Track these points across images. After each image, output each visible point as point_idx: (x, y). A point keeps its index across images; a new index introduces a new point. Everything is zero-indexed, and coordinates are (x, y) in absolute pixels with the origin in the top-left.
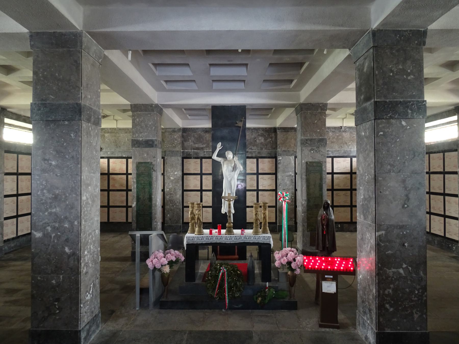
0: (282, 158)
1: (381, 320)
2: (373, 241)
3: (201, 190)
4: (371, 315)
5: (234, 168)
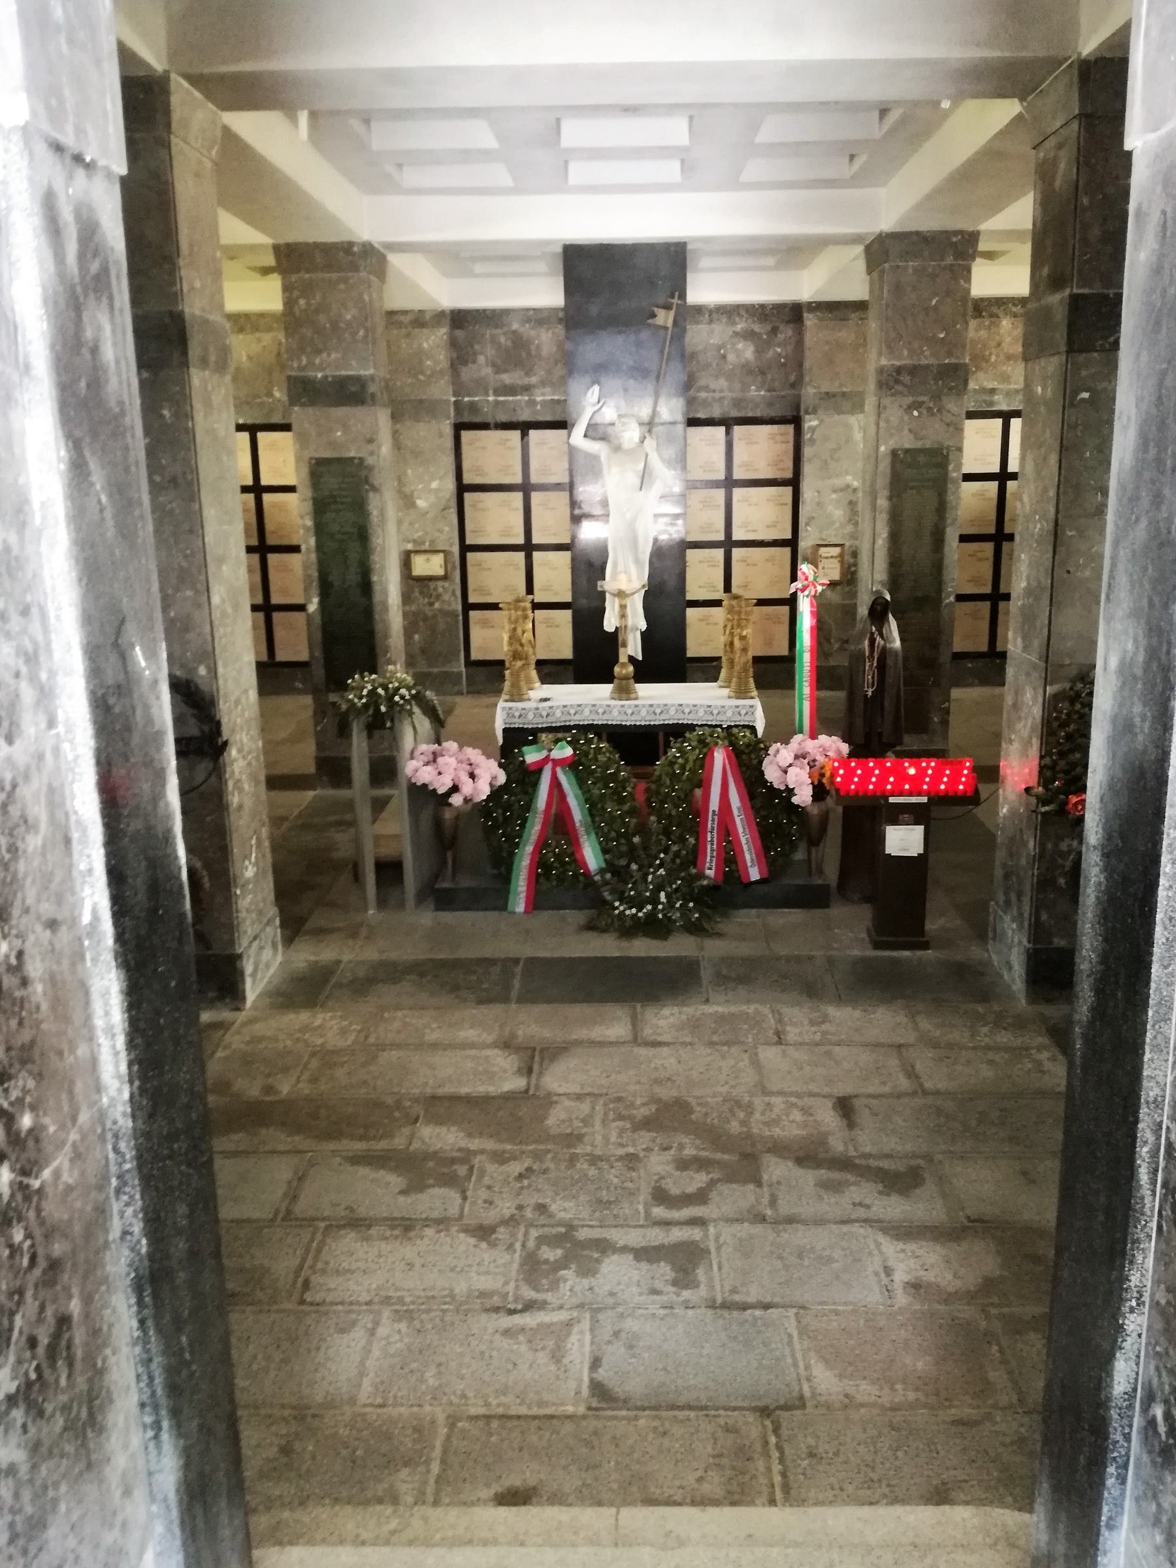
0: (821, 421)
1: (1044, 917)
2: (1037, 712)
3: (528, 548)
4: (1019, 908)
5: (645, 478)
